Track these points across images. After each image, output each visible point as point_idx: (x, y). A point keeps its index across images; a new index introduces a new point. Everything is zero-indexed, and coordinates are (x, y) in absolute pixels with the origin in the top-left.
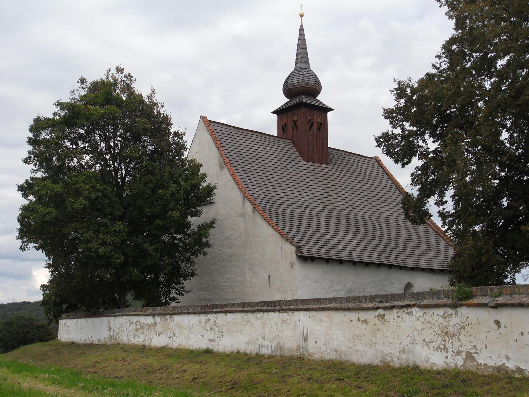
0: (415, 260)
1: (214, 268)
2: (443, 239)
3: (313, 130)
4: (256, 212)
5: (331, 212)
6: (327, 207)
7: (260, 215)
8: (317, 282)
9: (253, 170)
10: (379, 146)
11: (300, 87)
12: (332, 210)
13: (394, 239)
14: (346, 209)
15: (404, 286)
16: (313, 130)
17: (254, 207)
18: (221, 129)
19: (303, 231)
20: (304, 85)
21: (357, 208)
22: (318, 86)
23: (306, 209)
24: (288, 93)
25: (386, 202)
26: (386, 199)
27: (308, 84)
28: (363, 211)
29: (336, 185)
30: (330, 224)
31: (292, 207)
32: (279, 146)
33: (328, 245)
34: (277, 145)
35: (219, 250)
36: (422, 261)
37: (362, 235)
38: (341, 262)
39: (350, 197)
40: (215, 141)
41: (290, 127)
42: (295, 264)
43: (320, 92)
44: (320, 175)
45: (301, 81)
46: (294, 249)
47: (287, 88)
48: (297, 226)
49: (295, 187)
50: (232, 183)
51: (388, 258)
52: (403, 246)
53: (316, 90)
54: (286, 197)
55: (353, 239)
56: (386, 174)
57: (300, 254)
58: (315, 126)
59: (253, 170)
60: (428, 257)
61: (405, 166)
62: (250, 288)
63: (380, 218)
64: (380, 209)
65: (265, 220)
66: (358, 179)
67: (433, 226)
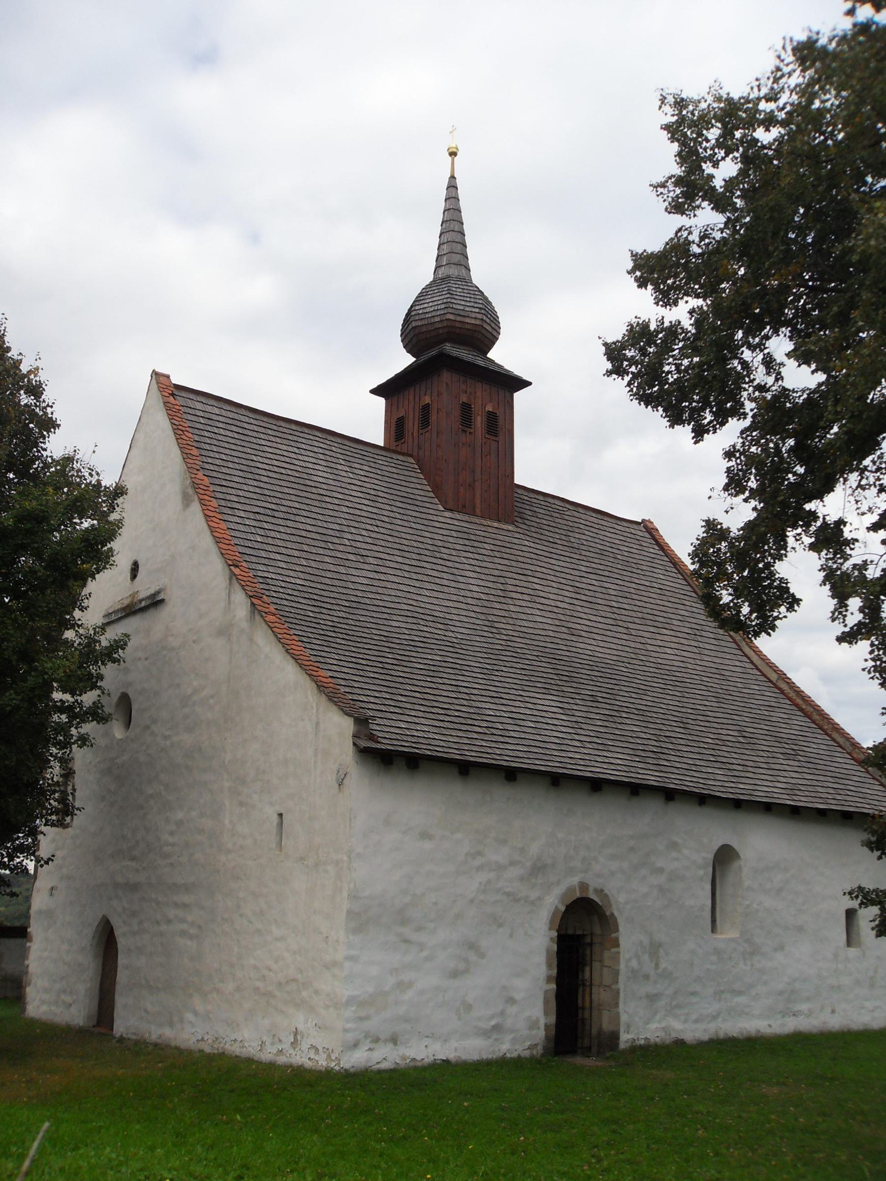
0: (743, 780)
1: (150, 791)
2: (821, 728)
3: (472, 431)
4: (258, 617)
5: (505, 638)
6: (496, 625)
7: (266, 627)
8: (425, 835)
9: (281, 515)
10: (617, 370)
11: (441, 321)
12: (511, 633)
13: (685, 720)
14: (551, 634)
15: (711, 856)
16: (472, 431)
17: (253, 604)
18: (209, 408)
19: (401, 680)
20: (451, 317)
21: (583, 634)
22: (488, 321)
23: (431, 624)
24: (411, 339)
25: (667, 626)
26: (669, 621)
27: (462, 313)
28: (602, 644)
29: (530, 573)
30: (496, 668)
31: (386, 616)
32: (377, 466)
33: (476, 723)
34: (372, 465)
35: (166, 738)
36: (765, 783)
37: (590, 704)
38: (511, 775)
39: (566, 606)
40: (178, 431)
41: (412, 426)
42: (348, 775)
43: (497, 339)
44: (486, 546)
45: (443, 306)
46: (347, 725)
47: (410, 327)
48: (387, 666)
49: (407, 568)
50: (207, 541)
51: (662, 768)
52: (710, 741)
53: (483, 331)
54: (373, 589)
55: (561, 711)
56: (671, 562)
57: (364, 744)
58: (479, 422)
59: (281, 515)
60: (780, 773)
61: (706, 435)
62: (229, 852)
63: (648, 664)
64: (649, 641)
65: (279, 640)
66: (593, 565)
67: (792, 695)
